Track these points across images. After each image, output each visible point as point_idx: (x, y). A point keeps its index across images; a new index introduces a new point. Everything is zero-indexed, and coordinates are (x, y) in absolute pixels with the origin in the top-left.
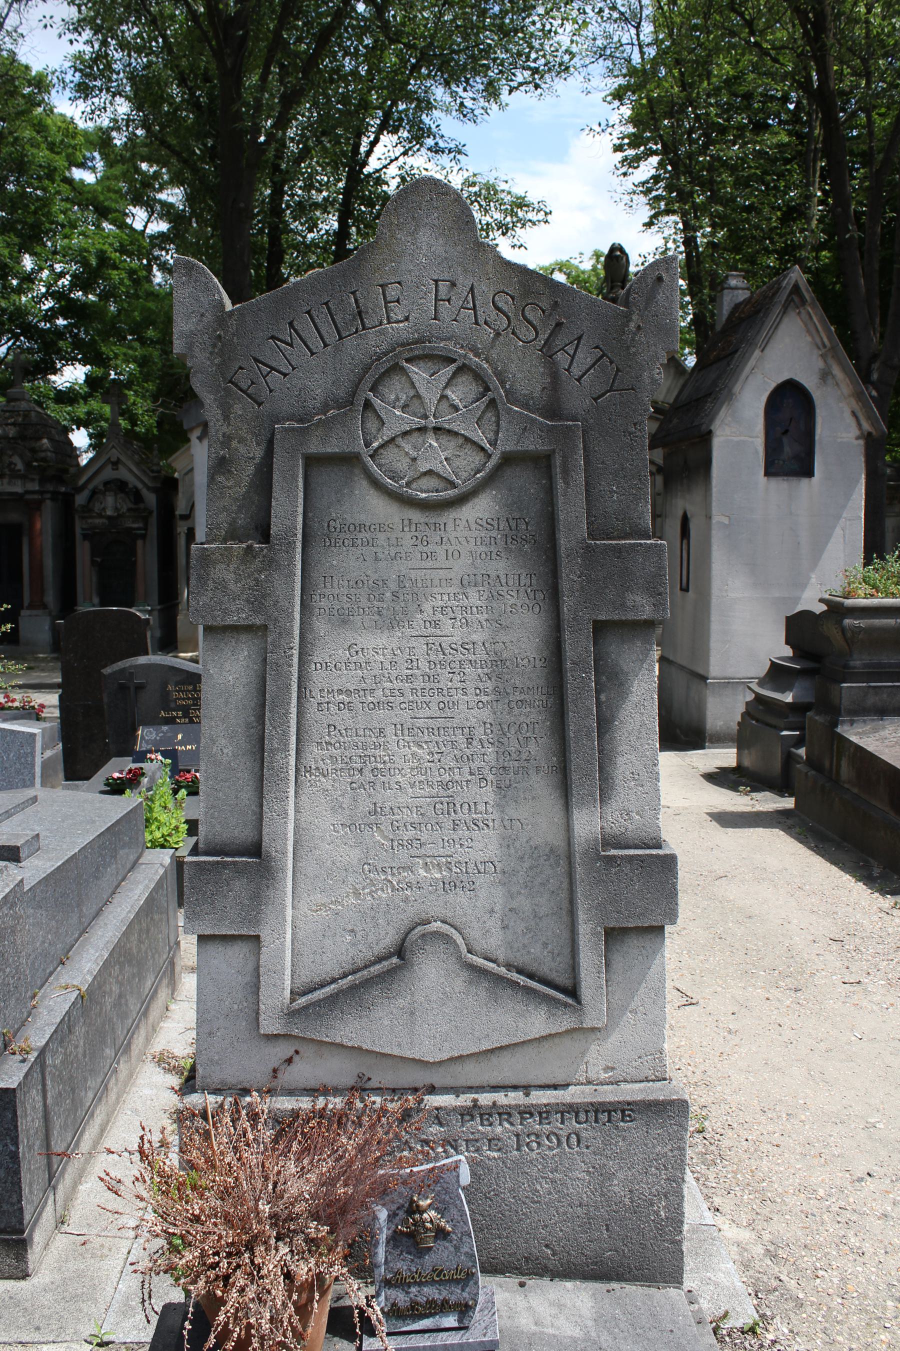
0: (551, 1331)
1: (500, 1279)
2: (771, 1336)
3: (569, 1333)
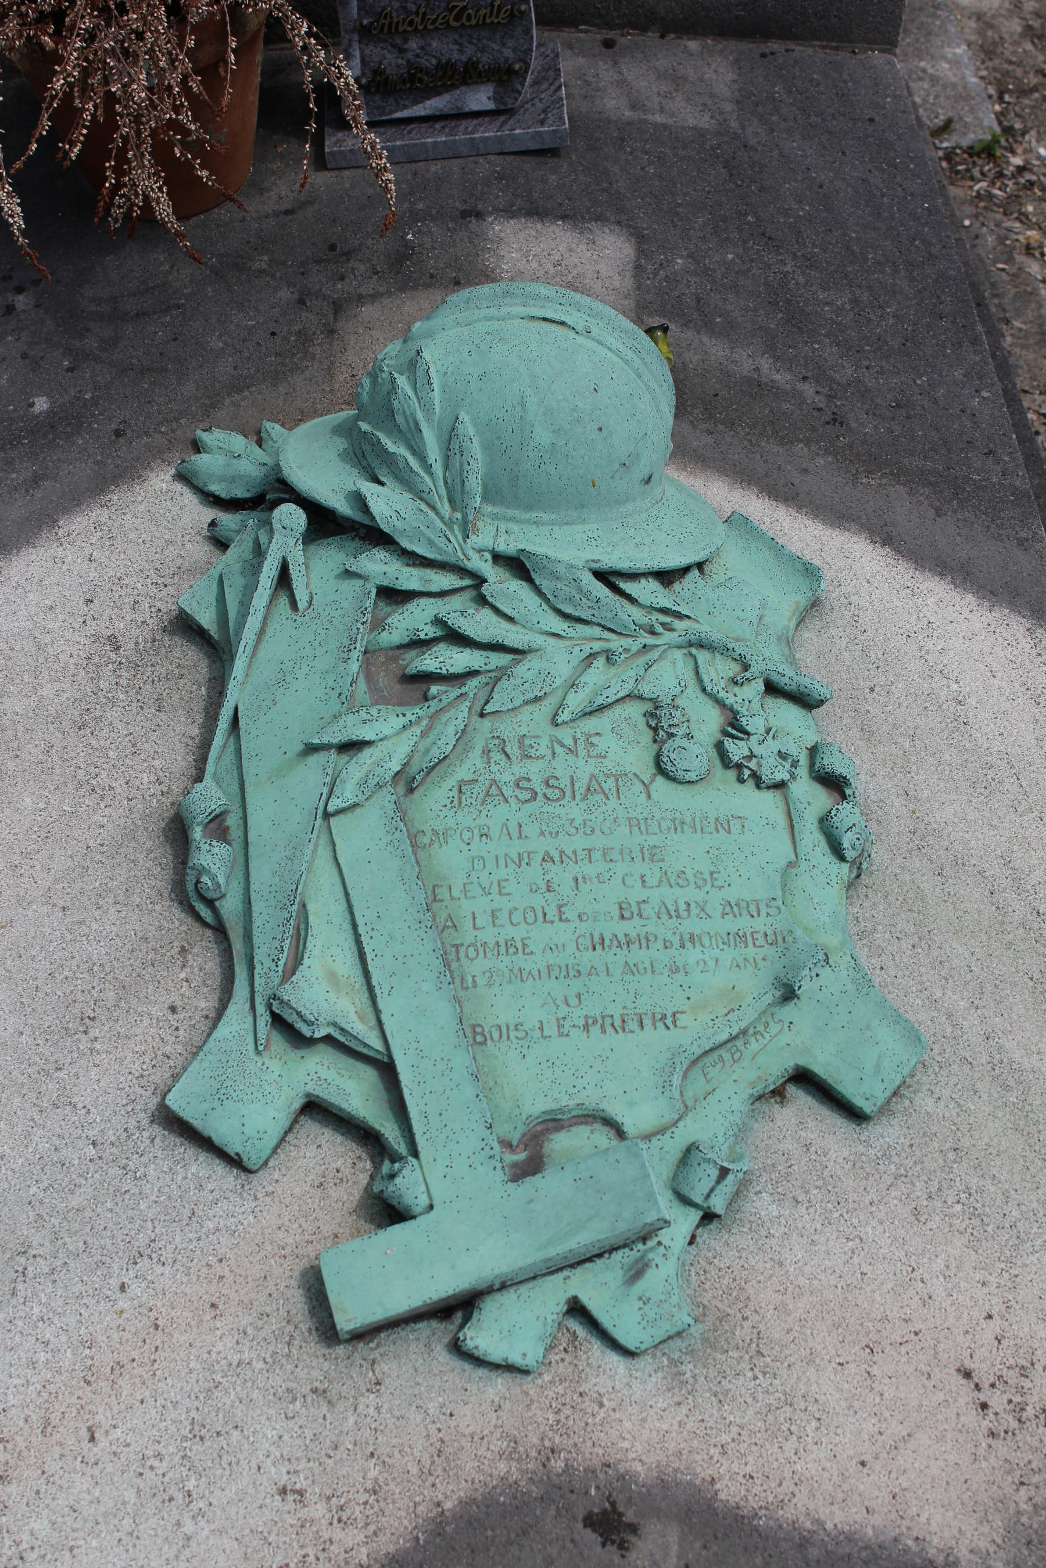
0: (659, 118)
1: (569, 34)
2: (1017, 161)
3: (691, 122)
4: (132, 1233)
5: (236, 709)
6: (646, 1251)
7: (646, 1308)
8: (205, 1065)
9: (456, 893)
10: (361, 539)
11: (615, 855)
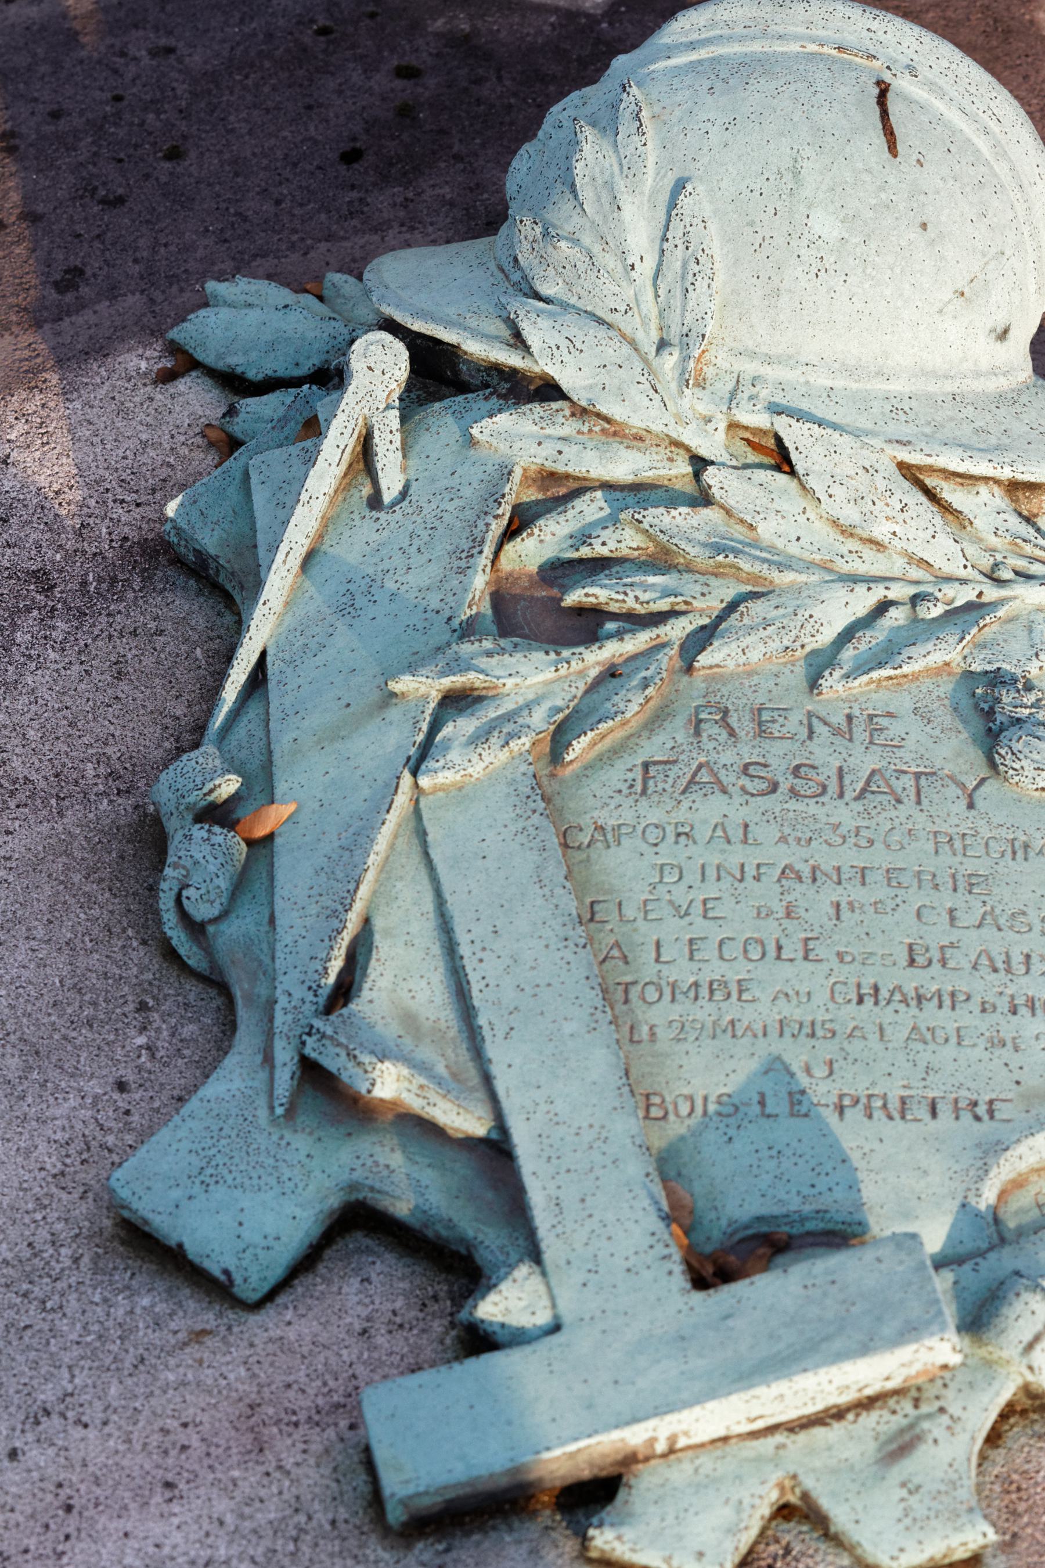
4: (35, 1382)
5: (263, 654)
6: (919, 1419)
7: (913, 1500)
8: (181, 1134)
9: (630, 912)
10: (500, 396)
11: (906, 879)
